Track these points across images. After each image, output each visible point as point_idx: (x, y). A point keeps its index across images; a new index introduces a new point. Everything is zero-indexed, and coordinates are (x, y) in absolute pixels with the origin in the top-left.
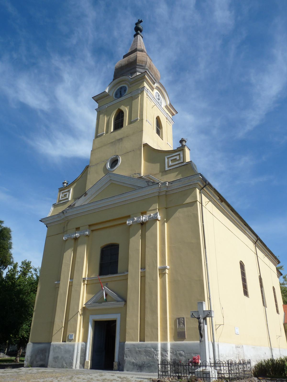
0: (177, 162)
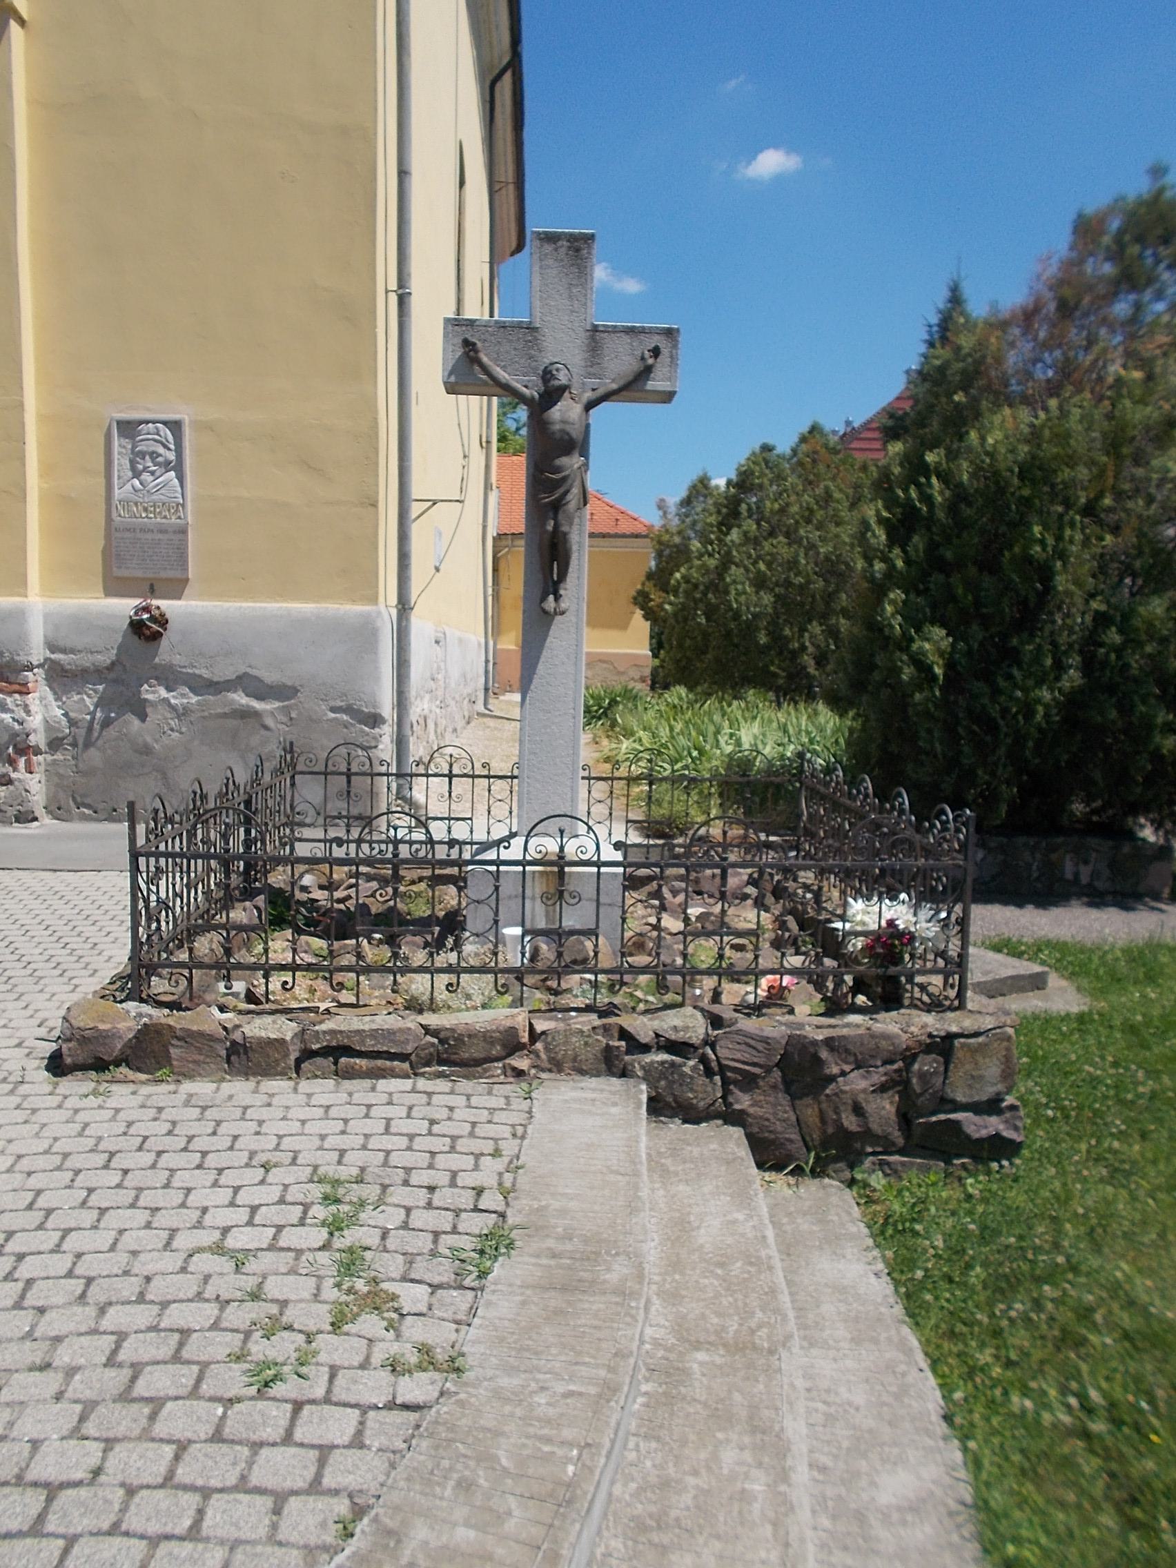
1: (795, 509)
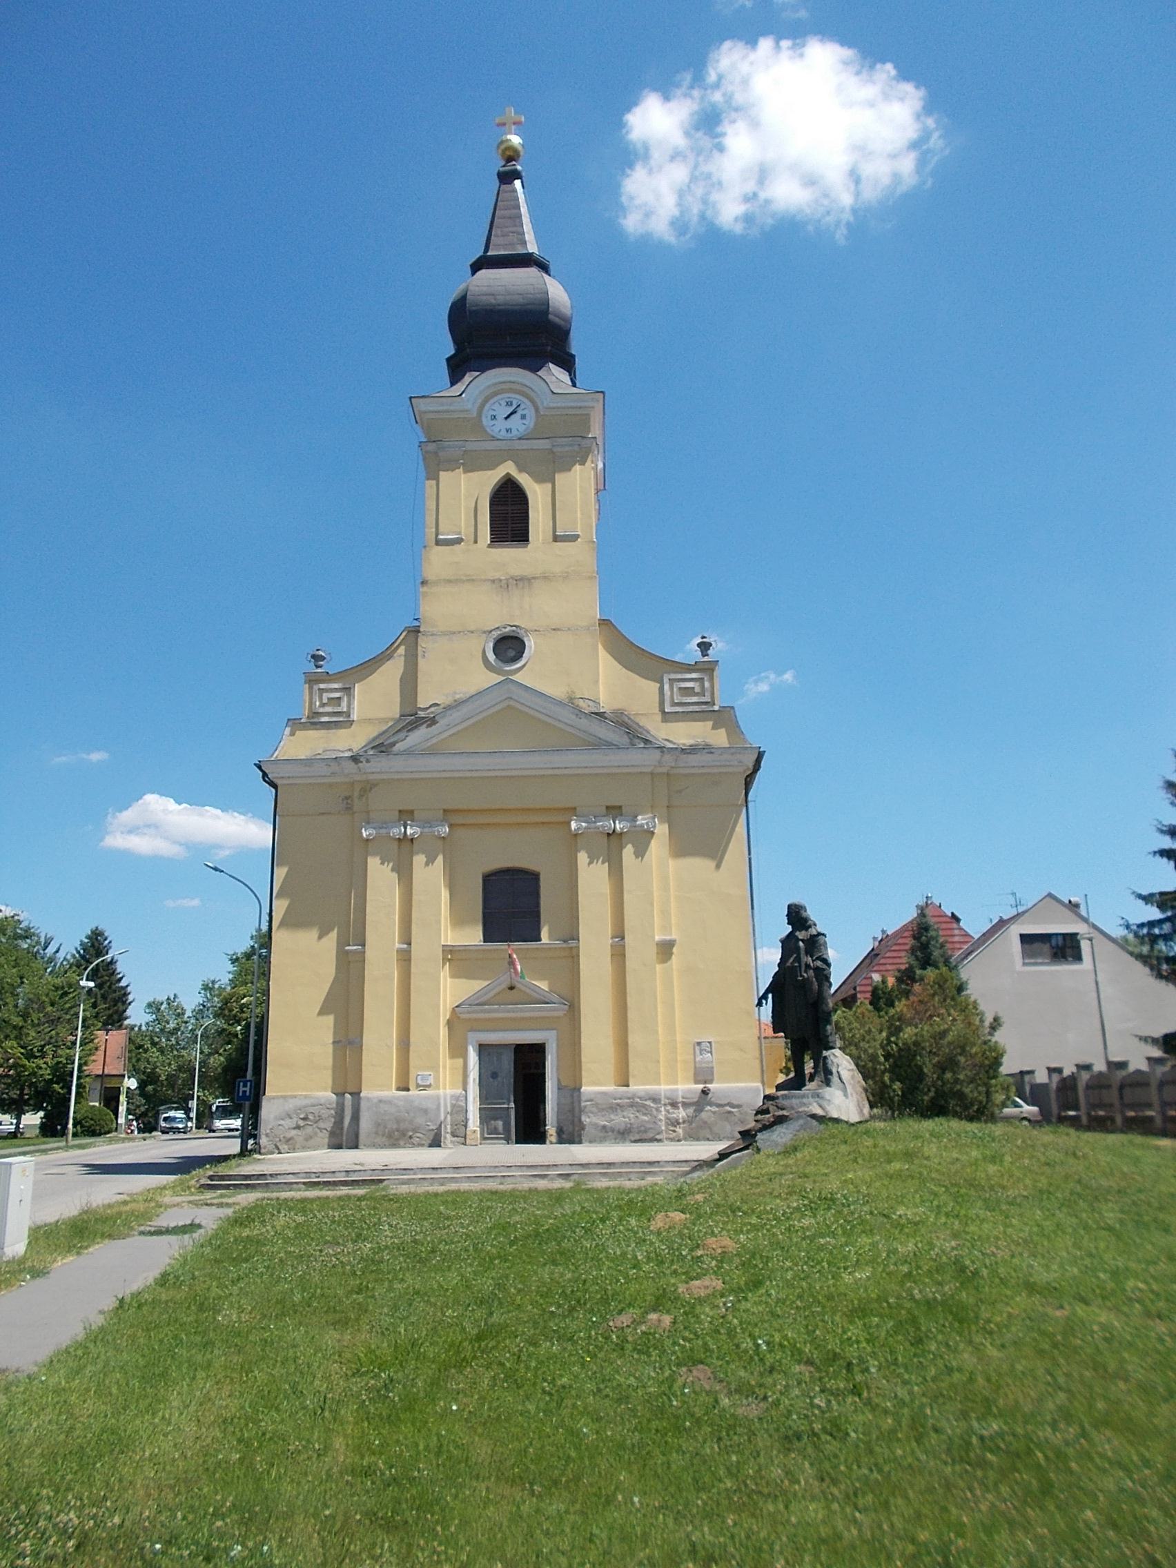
0: (695, 699)
1: (858, 1036)
